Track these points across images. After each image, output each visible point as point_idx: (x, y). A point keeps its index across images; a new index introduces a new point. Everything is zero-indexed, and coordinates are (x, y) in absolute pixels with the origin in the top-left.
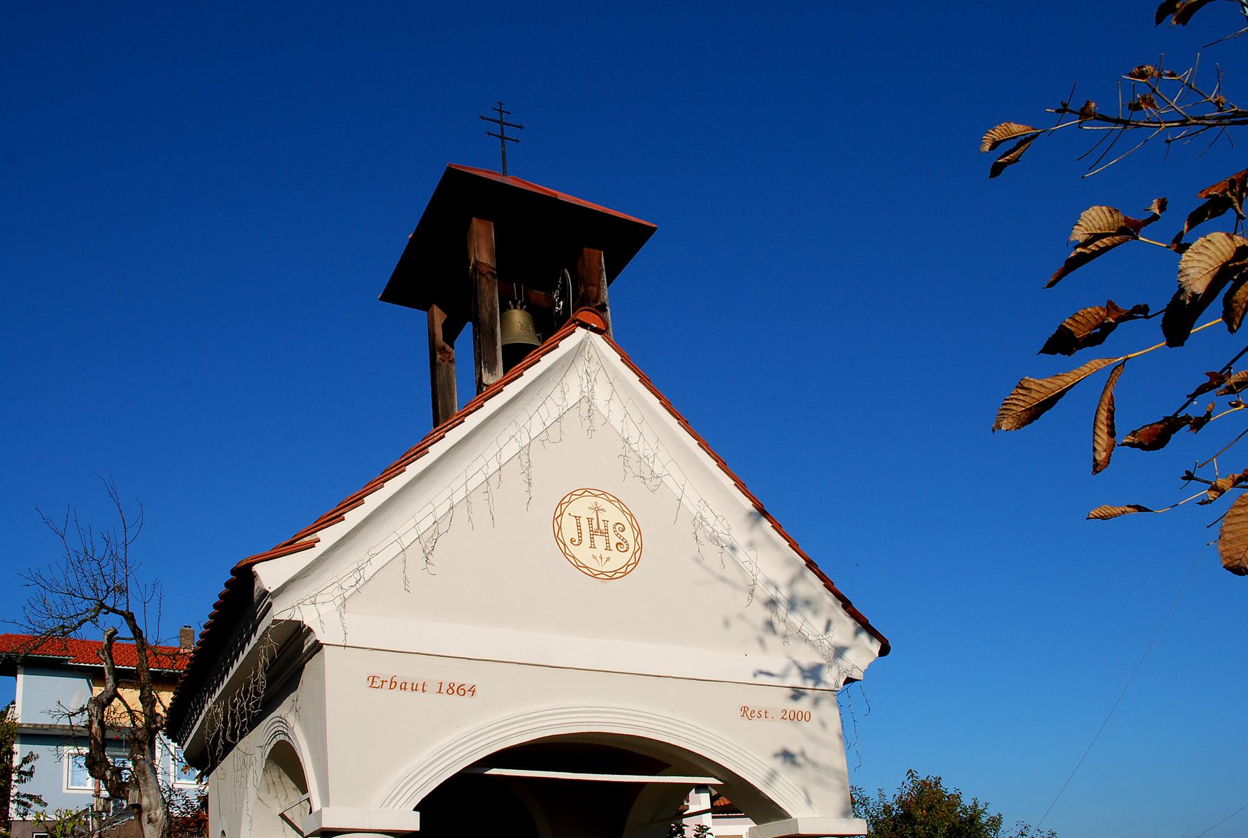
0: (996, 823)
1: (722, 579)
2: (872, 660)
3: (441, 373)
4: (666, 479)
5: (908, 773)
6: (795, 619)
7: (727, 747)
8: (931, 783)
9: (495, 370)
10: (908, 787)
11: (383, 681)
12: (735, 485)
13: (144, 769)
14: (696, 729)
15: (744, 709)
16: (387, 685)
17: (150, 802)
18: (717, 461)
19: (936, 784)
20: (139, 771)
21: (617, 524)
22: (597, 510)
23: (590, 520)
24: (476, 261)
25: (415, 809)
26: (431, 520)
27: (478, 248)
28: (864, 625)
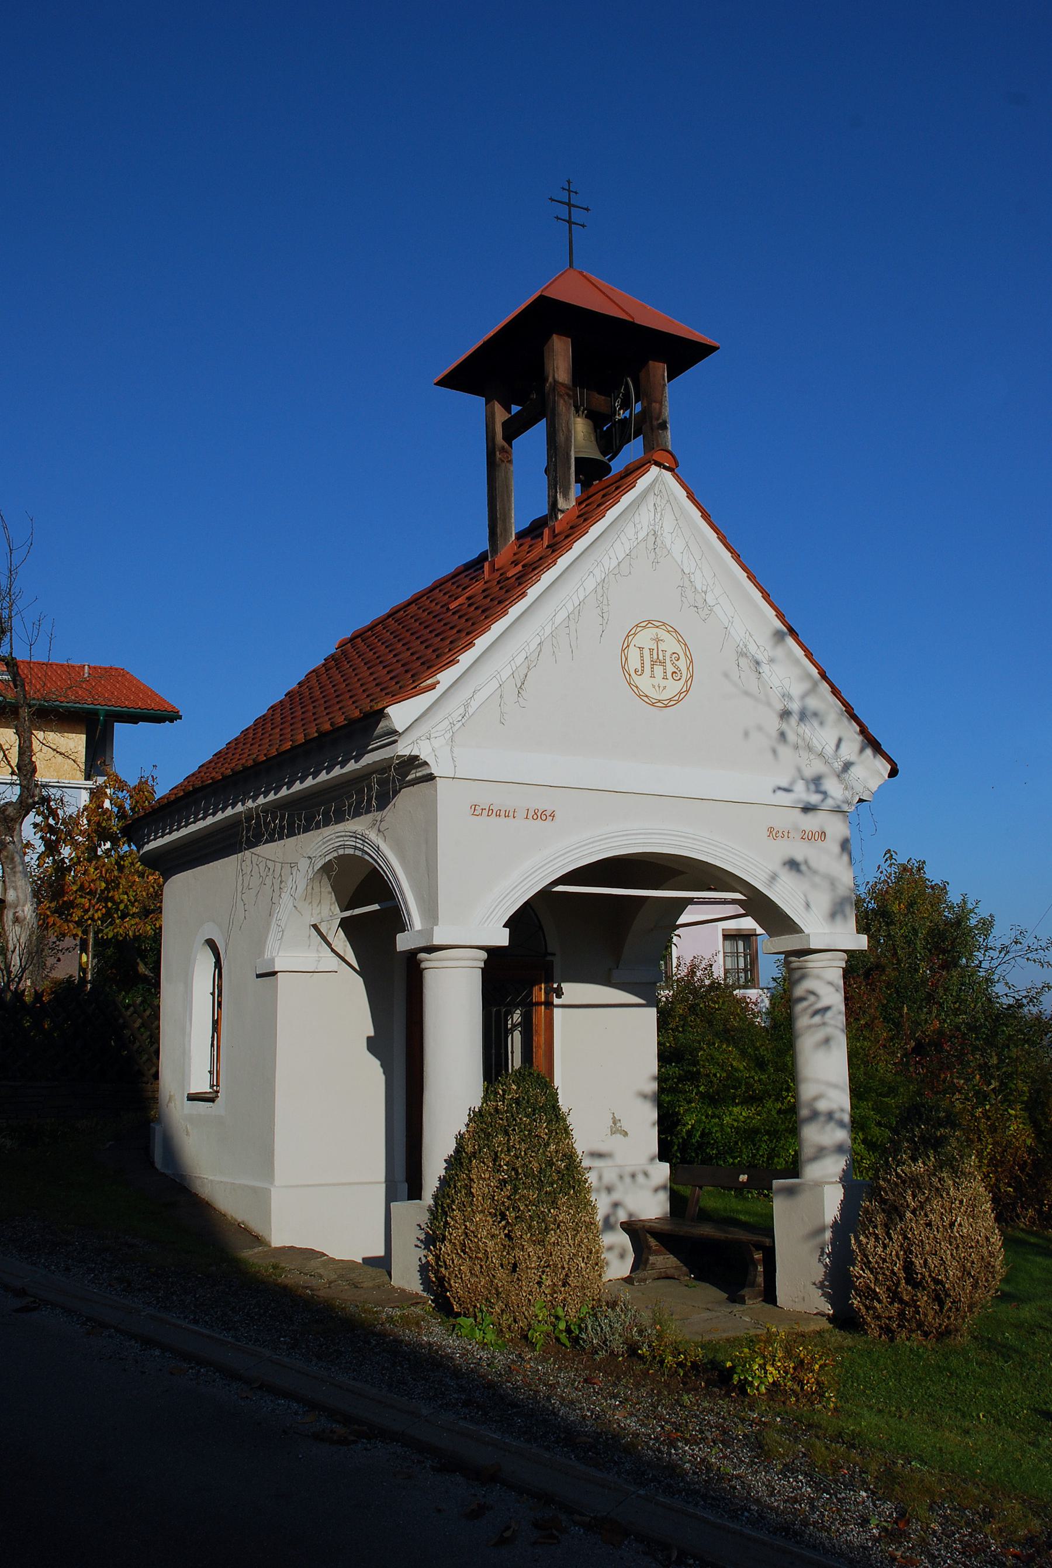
1: (746, 693)
3: (500, 475)
4: (717, 609)
5: (886, 854)
6: (805, 729)
7: (755, 865)
8: (912, 868)
10: (885, 872)
11: (482, 809)
12: (776, 615)
13: (12, 855)
14: (730, 849)
15: (771, 830)
16: (485, 812)
17: (17, 897)
18: (762, 593)
19: (919, 869)
21: (674, 653)
22: (658, 640)
24: (555, 380)
25: (504, 926)
27: (557, 368)
28: (872, 743)
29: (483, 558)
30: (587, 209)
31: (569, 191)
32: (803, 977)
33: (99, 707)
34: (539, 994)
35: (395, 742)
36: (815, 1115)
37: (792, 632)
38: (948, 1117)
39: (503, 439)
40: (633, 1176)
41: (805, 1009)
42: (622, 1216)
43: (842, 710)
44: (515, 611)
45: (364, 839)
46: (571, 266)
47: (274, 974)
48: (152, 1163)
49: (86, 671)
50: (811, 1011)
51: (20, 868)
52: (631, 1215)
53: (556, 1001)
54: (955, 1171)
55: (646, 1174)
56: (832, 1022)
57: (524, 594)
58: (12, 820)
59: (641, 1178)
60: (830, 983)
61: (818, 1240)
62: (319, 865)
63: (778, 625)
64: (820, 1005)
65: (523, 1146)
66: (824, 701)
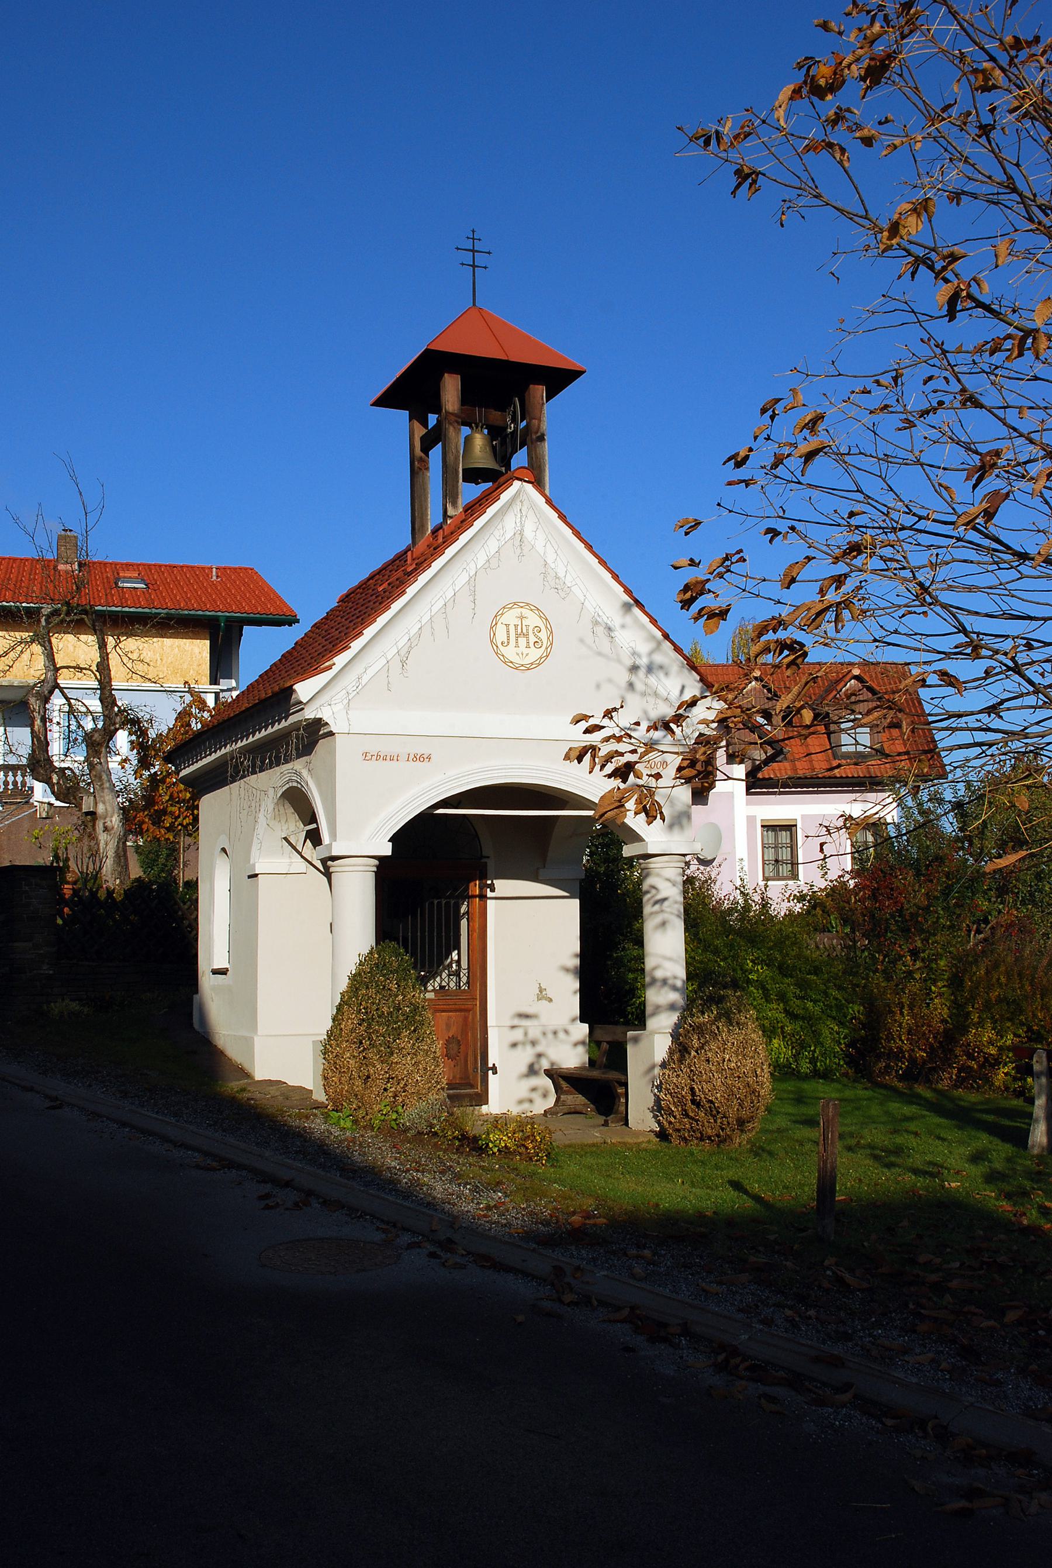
1: (600, 654)
6: (652, 680)
13: (100, 774)
16: (374, 758)
20: (95, 776)
22: (522, 618)
23: (516, 626)
26: (406, 638)
29: (408, 549)
31: (473, 239)
32: (648, 875)
33: (220, 614)
34: (475, 888)
35: (303, 709)
36: (654, 981)
37: (638, 603)
38: (732, 981)
39: (421, 450)
40: (555, 1033)
41: (649, 900)
42: (545, 1064)
43: (683, 663)
44: (396, 606)
45: (300, 775)
46: (474, 304)
47: (256, 875)
48: (192, 1025)
49: (214, 574)
50: (652, 901)
51: (107, 785)
52: (552, 1064)
53: (489, 894)
54: (730, 1022)
55: (566, 1032)
56: (668, 910)
57: (404, 592)
58: (98, 744)
59: (561, 1035)
60: (668, 880)
61: (651, 1075)
62: (281, 793)
63: (626, 598)
64: (659, 897)
65: (379, 996)
66: (667, 656)
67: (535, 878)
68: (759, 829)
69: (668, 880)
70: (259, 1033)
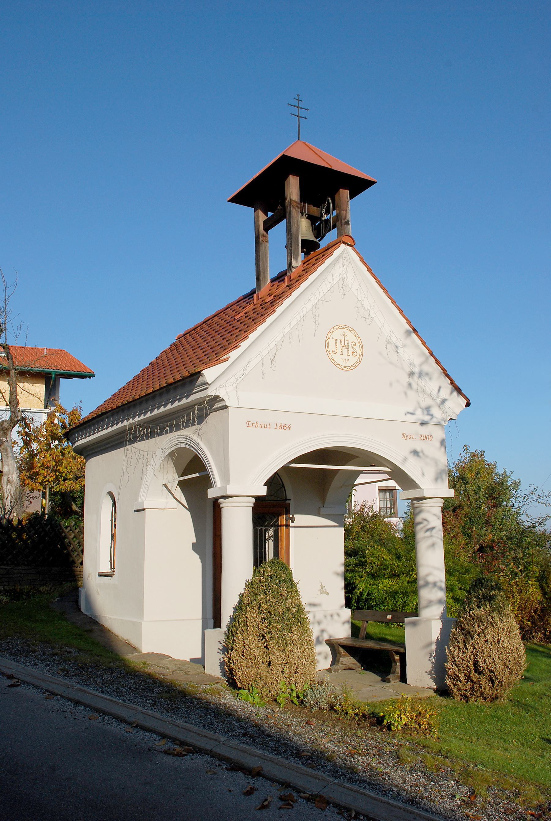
0: (517, 484)
1: (391, 363)
2: (461, 410)
3: (262, 248)
6: (422, 382)
9: (298, 259)
13: (6, 448)
15: (404, 434)
16: (254, 425)
22: (344, 335)
26: (274, 343)
30: (307, 110)
32: (420, 512)
33: (52, 370)
34: (282, 520)
36: (427, 584)
37: (415, 330)
40: (332, 616)
41: (422, 528)
42: (326, 637)
48: (80, 609)
51: (10, 454)
52: (330, 636)
54: (500, 613)
55: (338, 615)
56: (436, 535)
58: (6, 429)
59: (335, 617)
60: (435, 515)
61: (428, 649)
62: (169, 452)
63: (408, 327)
64: (429, 526)
65: (274, 600)
67: (318, 514)
68: (378, 491)
69: (435, 515)
70: (145, 619)
